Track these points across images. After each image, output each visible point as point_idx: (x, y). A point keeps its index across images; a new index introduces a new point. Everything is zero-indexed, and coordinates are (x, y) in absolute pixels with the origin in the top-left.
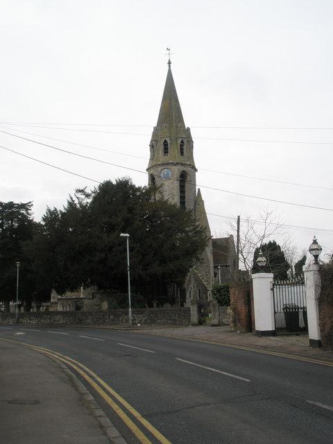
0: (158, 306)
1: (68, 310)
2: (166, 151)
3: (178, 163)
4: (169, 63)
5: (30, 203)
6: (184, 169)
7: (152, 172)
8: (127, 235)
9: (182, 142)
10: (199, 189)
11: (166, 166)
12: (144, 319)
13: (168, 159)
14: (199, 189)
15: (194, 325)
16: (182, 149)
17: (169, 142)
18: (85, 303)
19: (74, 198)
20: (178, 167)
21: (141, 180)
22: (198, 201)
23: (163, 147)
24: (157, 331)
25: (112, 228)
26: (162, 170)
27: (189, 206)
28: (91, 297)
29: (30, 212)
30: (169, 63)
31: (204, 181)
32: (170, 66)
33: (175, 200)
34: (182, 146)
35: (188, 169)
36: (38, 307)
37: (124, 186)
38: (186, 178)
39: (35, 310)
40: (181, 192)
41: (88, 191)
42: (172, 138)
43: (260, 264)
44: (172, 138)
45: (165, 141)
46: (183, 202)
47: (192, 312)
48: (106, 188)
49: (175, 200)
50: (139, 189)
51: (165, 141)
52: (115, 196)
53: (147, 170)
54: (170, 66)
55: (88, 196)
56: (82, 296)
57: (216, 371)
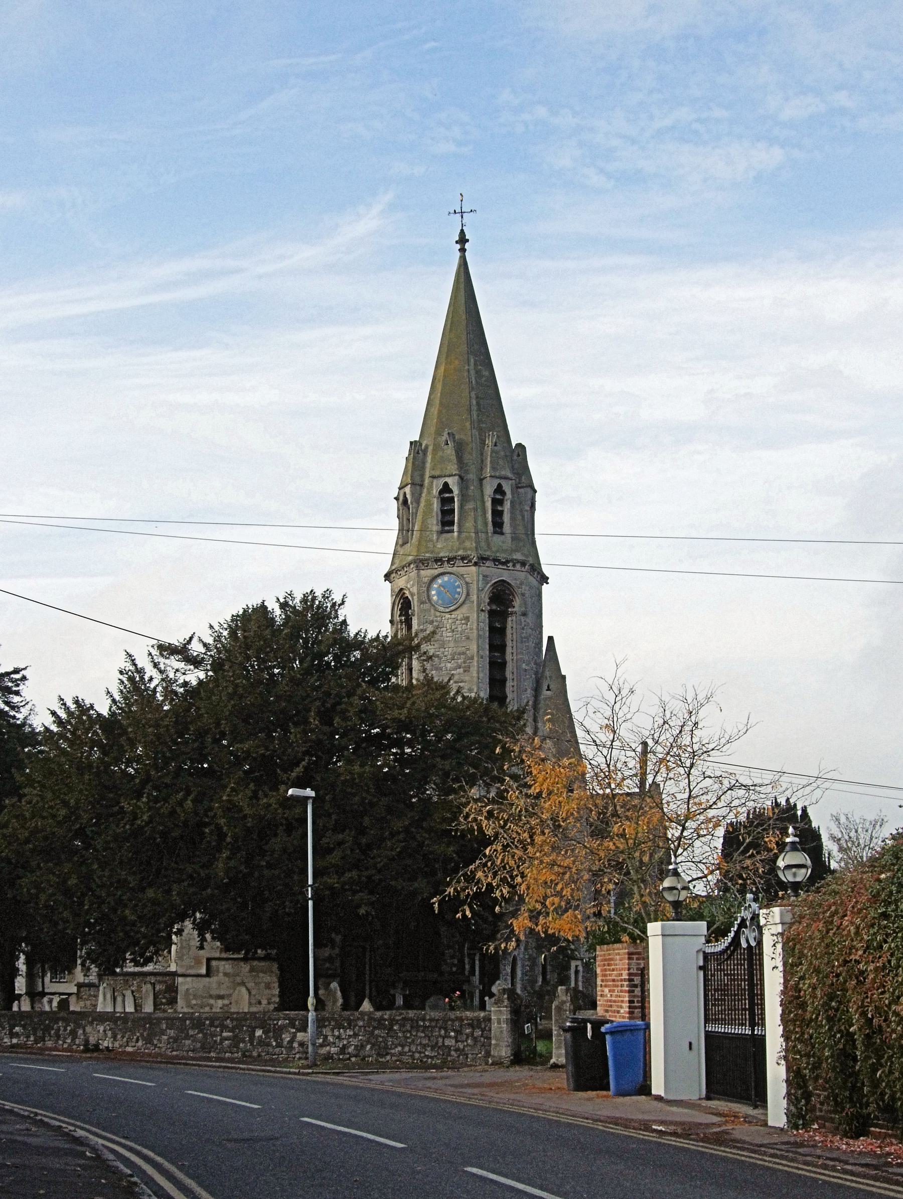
0: (408, 1005)
1: (130, 1009)
2: (446, 522)
3: (483, 559)
4: (463, 240)
5: (16, 671)
6: (505, 576)
7: (401, 582)
8: (309, 792)
9: (499, 490)
10: (551, 639)
11: (447, 568)
12: (354, 1042)
13: (444, 546)
14: (551, 639)
15: (498, 1063)
16: (497, 515)
17: (456, 491)
18: (182, 989)
19: (150, 671)
20: (489, 569)
21: (369, 616)
22: (547, 670)
23: (436, 505)
24: (672, 1109)
25: (268, 773)
26: (434, 578)
27: (517, 694)
28: (203, 971)
29: (16, 699)
30: (463, 240)
31: (573, 620)
32: (463, 250)
33: (470, 683)
34: (496, 502)
35: (514, 576)
36: (291, 733)
37: (312, 619)
38: (511, 606)
39: (26, 1006)
40: (492, 648)
41: (196, 648)
42: (471, 479)
43: (787, 877)
44: (471, 479)
45: (446, 488)
46: (497, 682)
47: (495, 1026)
48: (252, 625)
49: (470, 683)
50: (358, 643)
51: (446, 488)
52: (282, 659)
53: (387, 577)
54: (463, 250)
55: (196, 662)
56: (173, 968)
57: (211, 1096)
